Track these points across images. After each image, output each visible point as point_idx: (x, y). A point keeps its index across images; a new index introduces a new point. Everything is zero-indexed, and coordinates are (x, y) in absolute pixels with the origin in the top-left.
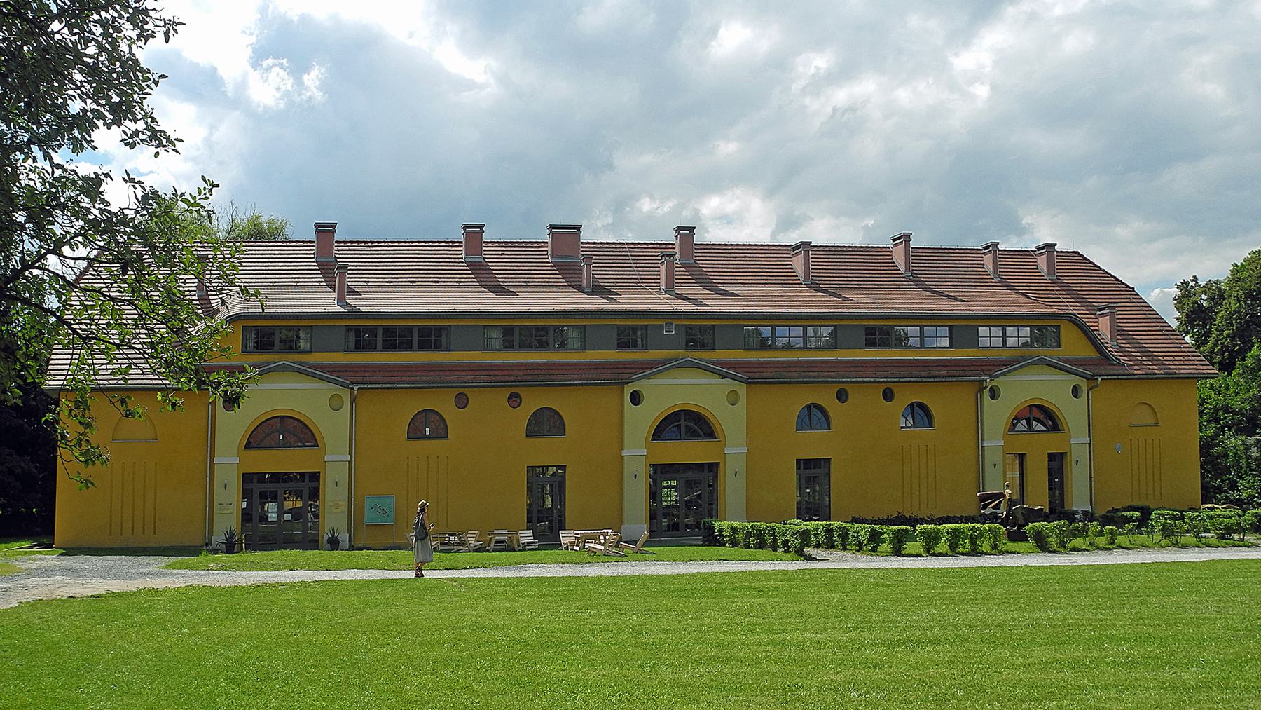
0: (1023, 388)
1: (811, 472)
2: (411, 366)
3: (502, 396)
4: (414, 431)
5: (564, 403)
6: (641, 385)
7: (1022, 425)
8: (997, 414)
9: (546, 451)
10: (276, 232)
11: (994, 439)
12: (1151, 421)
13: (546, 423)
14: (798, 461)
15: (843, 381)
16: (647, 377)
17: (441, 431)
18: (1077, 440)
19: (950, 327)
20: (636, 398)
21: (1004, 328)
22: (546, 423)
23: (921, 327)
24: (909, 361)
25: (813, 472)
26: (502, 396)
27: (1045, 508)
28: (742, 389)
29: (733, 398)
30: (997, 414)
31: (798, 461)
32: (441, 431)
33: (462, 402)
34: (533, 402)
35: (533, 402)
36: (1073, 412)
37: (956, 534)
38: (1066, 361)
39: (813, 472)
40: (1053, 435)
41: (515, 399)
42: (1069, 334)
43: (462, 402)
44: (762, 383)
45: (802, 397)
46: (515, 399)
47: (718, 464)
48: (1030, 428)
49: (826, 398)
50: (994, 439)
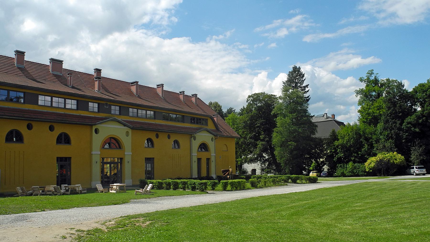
0: (109, 129)
1: (63, 163)
2: (6, 108)
3: (46, 127)
4: (9, 138)
5: (72, 132)
6: (99, 126)
7: (107, 146)
8: (98, 140)
9: (64, 151)
10: (342, 123)
11: (96, 152)
12: (226, 149)
13: (64, 139)
14: (57, 158)
15: (157, 130)
16: (100, 123)
17: (20, 138)
18: (212, 154)
19: (120, 107)
20: (97, 131)
21: (65, 99)
22: (64, 139)
23: (9, 91)
24: (93, 117)
25: (64, 163)
26: (47, 126)
27: (197, 177)
28: (130, 131)
29: (127, 134)
30: (98, 140)
31: (57, 158)
32: (20, 138)
33: (30, 127)
34: (59, 130)
35: (59, 130)
36: (211, 145)
37: (185, 183)
38: (124, 121)
39: (64, 163)
40: (207, 153)
41: (51, 129)
42: (210, 122)
43: (30, 127)
44: (63, 123)
45: (9, 126)
46: (51, 129)
47: (71, 158)
48: (202, 150)
49: (22, 128)
50: (96, 152)
